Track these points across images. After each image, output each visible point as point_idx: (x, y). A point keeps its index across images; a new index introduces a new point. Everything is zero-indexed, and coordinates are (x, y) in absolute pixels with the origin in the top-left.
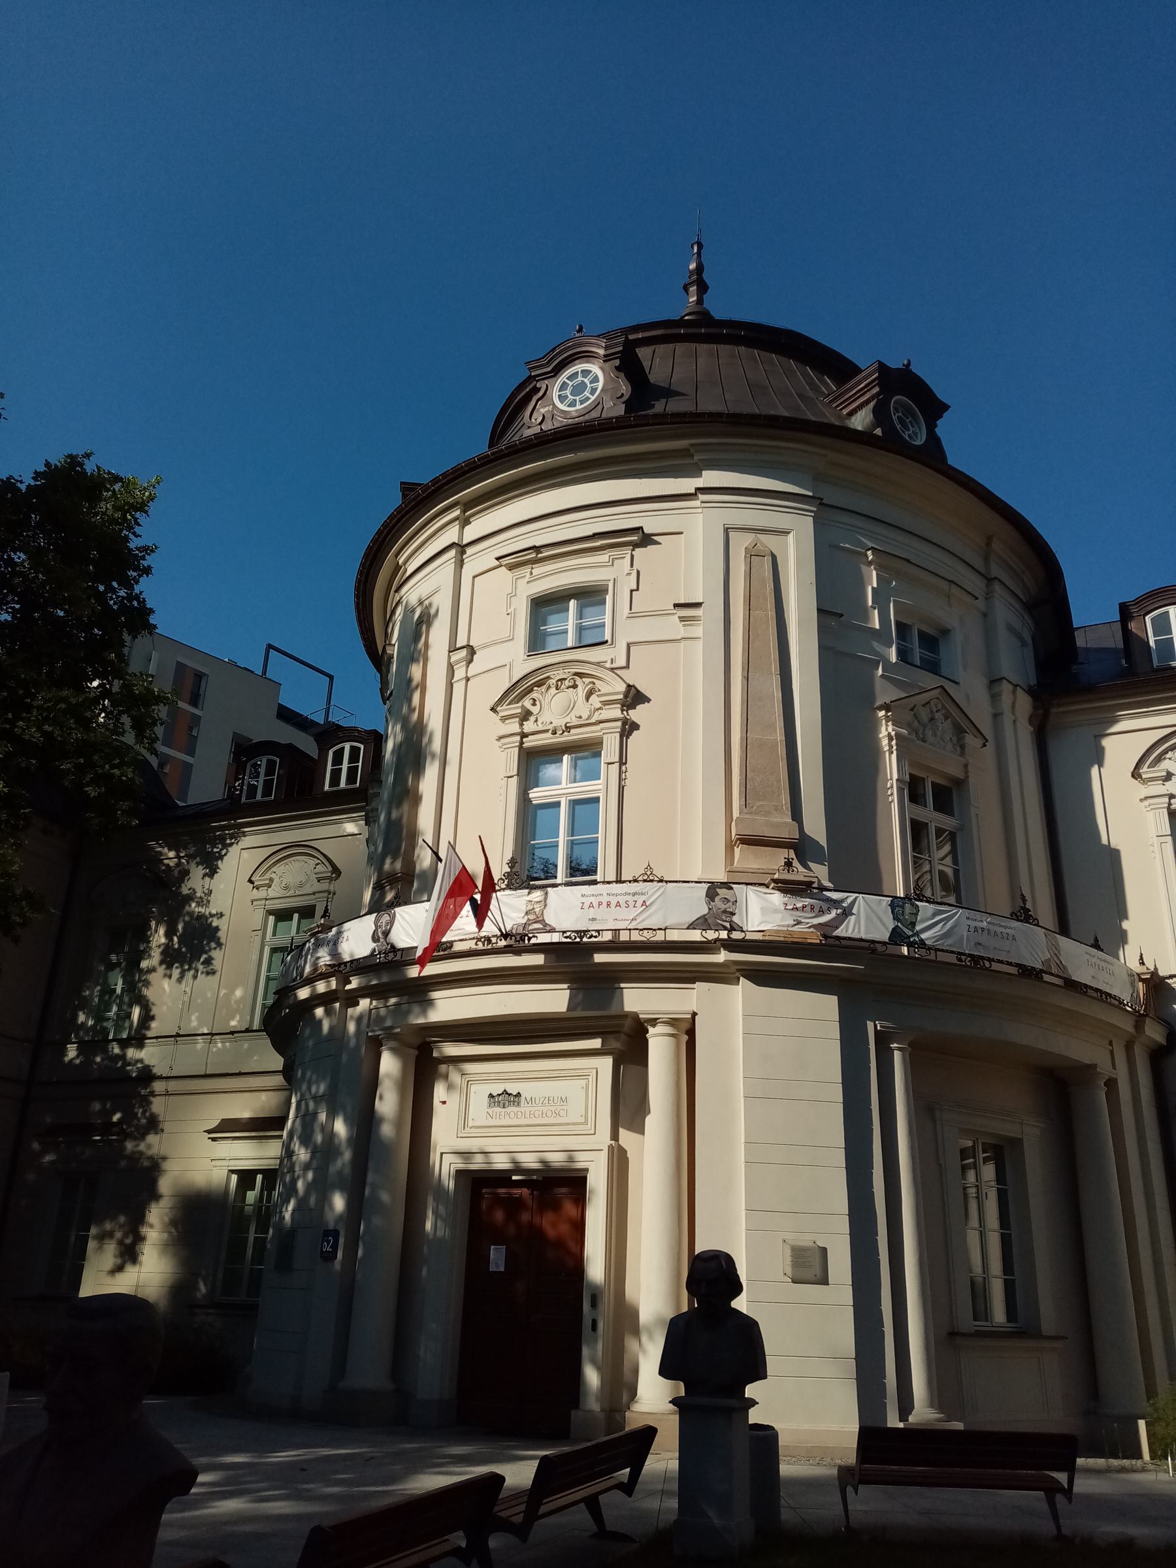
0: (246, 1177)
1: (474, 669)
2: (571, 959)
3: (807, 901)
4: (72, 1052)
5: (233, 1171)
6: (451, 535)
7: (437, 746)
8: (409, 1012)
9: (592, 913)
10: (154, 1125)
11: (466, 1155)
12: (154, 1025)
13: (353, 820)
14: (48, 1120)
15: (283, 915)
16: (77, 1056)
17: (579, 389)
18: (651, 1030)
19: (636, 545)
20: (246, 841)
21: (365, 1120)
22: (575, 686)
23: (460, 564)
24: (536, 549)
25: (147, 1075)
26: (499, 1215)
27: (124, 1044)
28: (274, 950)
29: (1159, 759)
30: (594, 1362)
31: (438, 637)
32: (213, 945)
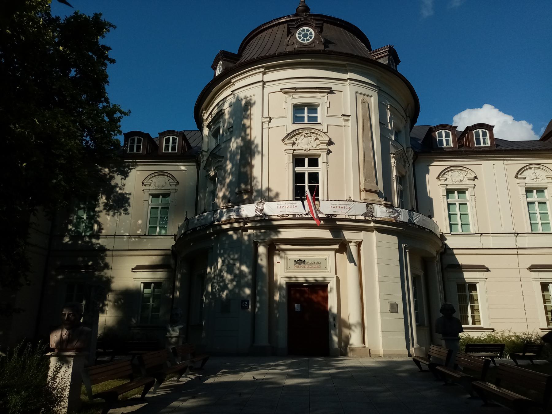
0: (147, 285)
1: (271, 125)
2: (330, 222)
3: (392, 210)
4: (67, 239)
5: (142, 283)
6: (259, 77)
7: (260, 149)
8: (270, 234)
9: (334, 209)
10: (107, 266)
11: (290, 278)
12: (103, 231)
13: (183, 165)
14: (58, 263)
15: (155, 196)
16: (69, 241)
17: (305, 36)
18: (350, 244)
19: (328, 93)
20: (139, 168)
21: (255, 267)
22: (311, 136)
23: (263, 88)
24: (296, 88)
25: (103, 249)
26: (298, 295)
27: (91, 237)
28: (152, 208)
29: (444, 174)
30: (336, 335)
31: (255, 111)
32: (127, 205)
